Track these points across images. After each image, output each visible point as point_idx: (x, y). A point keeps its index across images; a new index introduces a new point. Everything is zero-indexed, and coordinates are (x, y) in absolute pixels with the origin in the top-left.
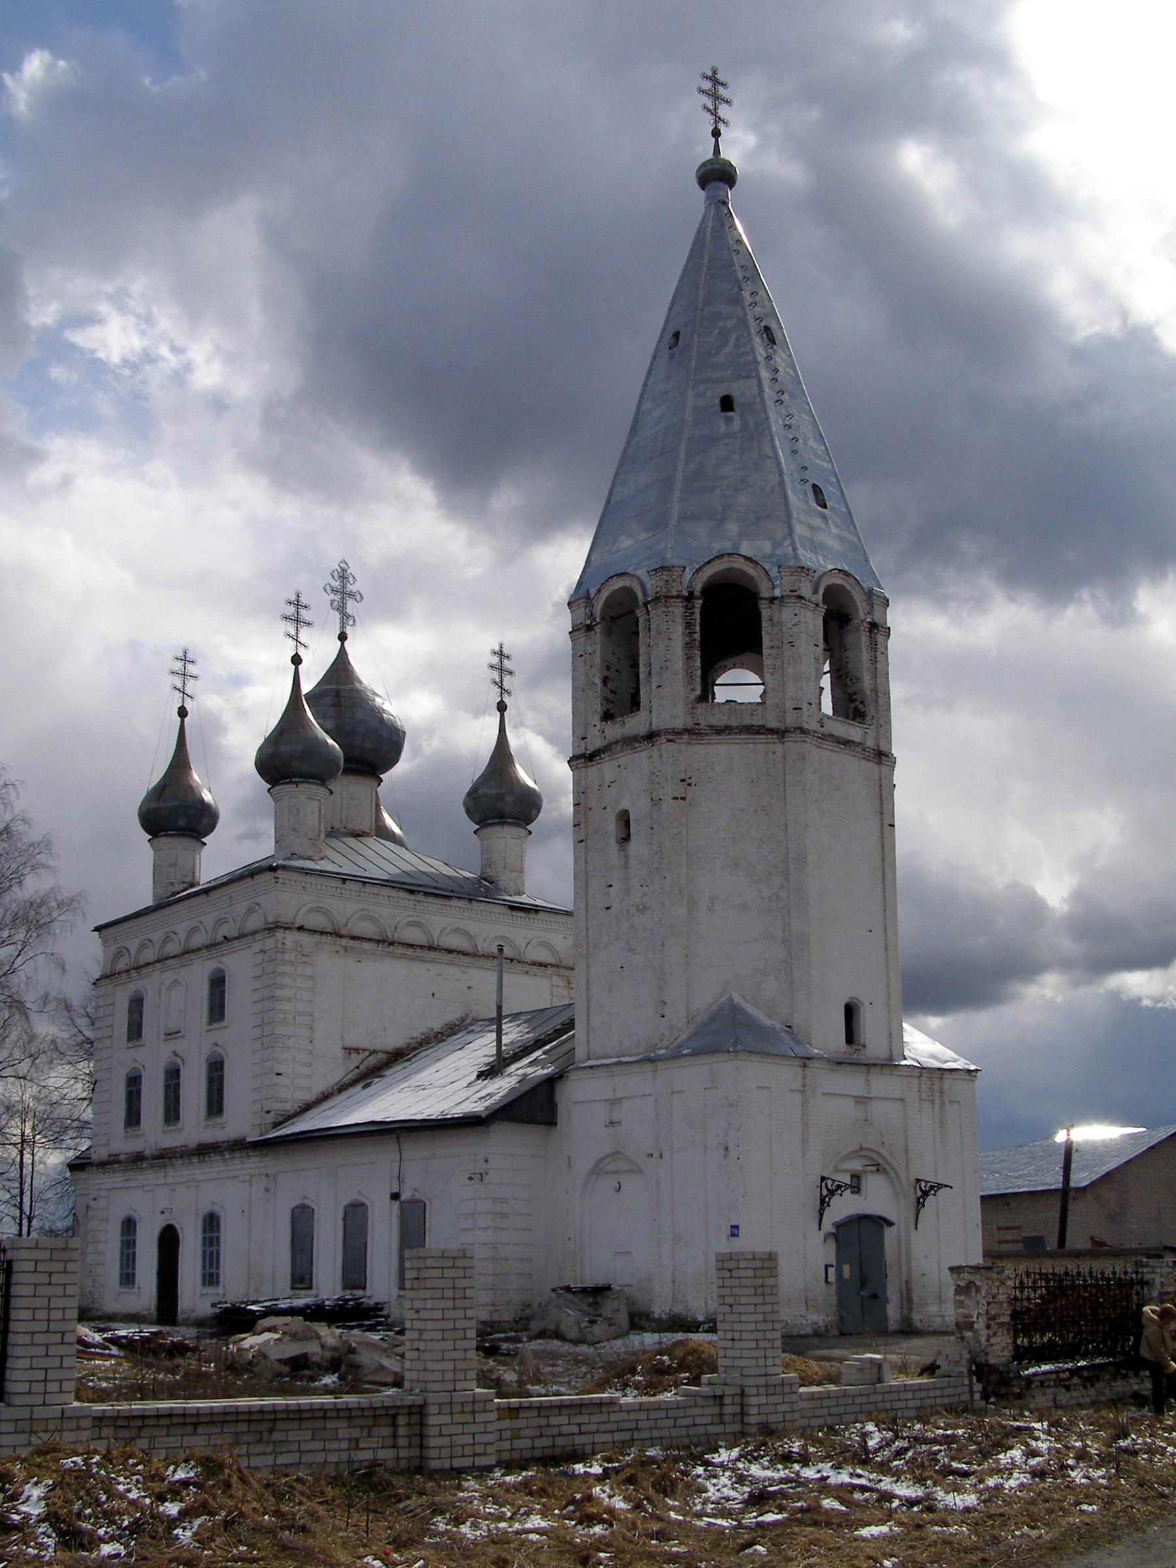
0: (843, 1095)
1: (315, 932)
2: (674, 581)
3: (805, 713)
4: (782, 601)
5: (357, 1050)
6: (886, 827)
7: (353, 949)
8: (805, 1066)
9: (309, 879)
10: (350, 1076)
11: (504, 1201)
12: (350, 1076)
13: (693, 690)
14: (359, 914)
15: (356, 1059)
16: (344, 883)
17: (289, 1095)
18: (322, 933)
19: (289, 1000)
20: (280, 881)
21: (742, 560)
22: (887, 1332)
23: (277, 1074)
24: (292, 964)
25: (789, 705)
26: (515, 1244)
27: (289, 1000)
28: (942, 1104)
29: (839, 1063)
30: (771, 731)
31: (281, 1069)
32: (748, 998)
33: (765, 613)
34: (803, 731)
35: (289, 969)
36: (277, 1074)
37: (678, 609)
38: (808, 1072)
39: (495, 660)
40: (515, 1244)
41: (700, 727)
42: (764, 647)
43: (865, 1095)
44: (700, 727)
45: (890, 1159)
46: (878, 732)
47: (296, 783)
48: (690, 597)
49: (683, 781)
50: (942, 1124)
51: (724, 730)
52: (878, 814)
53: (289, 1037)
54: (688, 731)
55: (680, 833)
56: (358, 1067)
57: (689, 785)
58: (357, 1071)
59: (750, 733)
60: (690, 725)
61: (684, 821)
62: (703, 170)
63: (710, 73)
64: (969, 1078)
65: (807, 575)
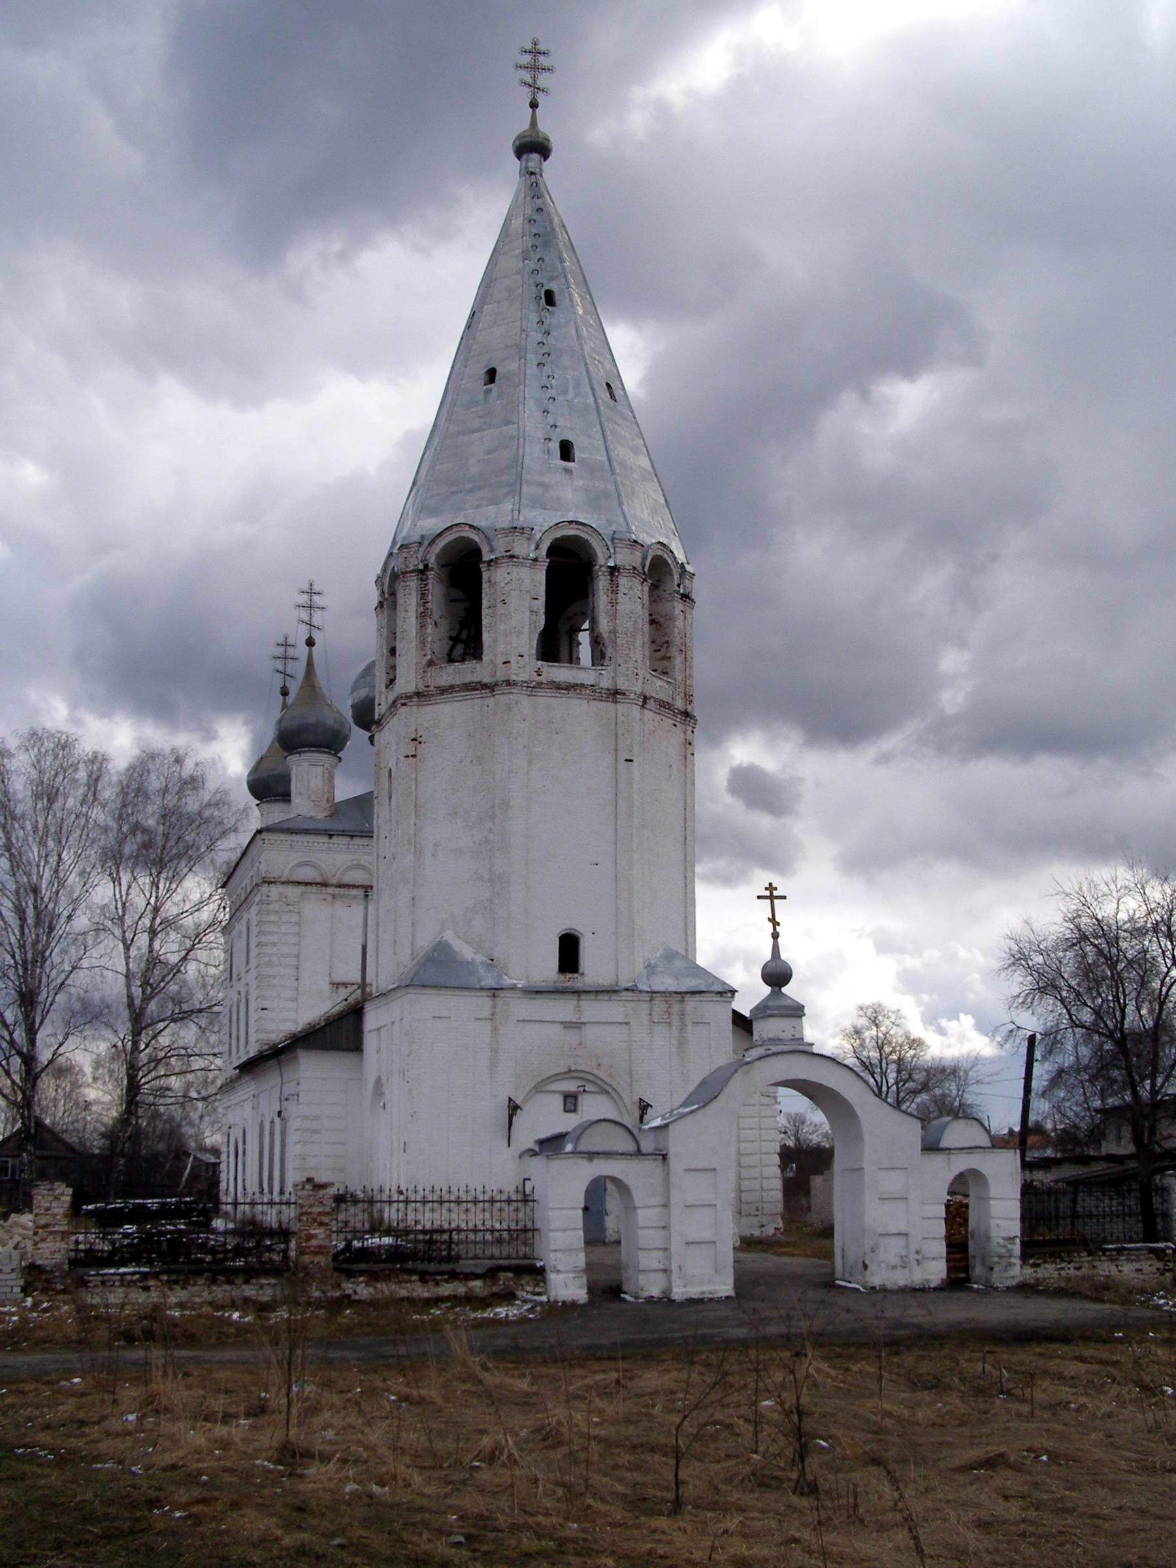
0: (536, 1021)
1: (299, 883)
2: (412, 556)
3: (514, 665)
4: (496, 563)
5: (345, 985)
6: (689, 756)
7: (342, 896)
8: (494, 996)
9: (295, 837)
10: (336, 1008)
11: (316, 1118)
12: (336, 1008)
13: (425, 655)
14: (349, 864)
15: (343, 993)
16: (330, 838)
17: (274, 1026)
18: (307, 884)
19: (274, 944)
20: (266, 841)
21: (467, 528)
22: (604, 1243)
23: (263, 1009)
24: (277, 912)
25: (500, 660)
26: (326, 1156)
27: (274, 944)
28: (682, 1027)
29: (537, 992)
30: (485, 686)
31: (265, 1004)
32: (461, 935)
33: (485, 576)
34: (508, 683)
35: (273, 918)
36: (263, 1009)
37: (413, 583)
38: (499, 1002)
39: (279, 651)
40: (326, 1156)
41: (430, 689)
42: (483, 607)
43: (574, 1020)
44: (430, 689)
45: (608, 1080)
46: (615, 671)
47: (299, 753)
48: (423, 572)
49: (413, 740)
50: (681, 1044)
51: (447, 690)
52: (612, 752)
53: (274, 977)
54: (418, 694)
55: (410, 788)
56: (346, 1000)
57: (420, 743)
58: (344, 1003)
59: (468, 690)
60: (421, 688)
61: (414, 776)
62: (517, 143)
63: (529, 46)
64: (720, 999)
65: (522, 533)
